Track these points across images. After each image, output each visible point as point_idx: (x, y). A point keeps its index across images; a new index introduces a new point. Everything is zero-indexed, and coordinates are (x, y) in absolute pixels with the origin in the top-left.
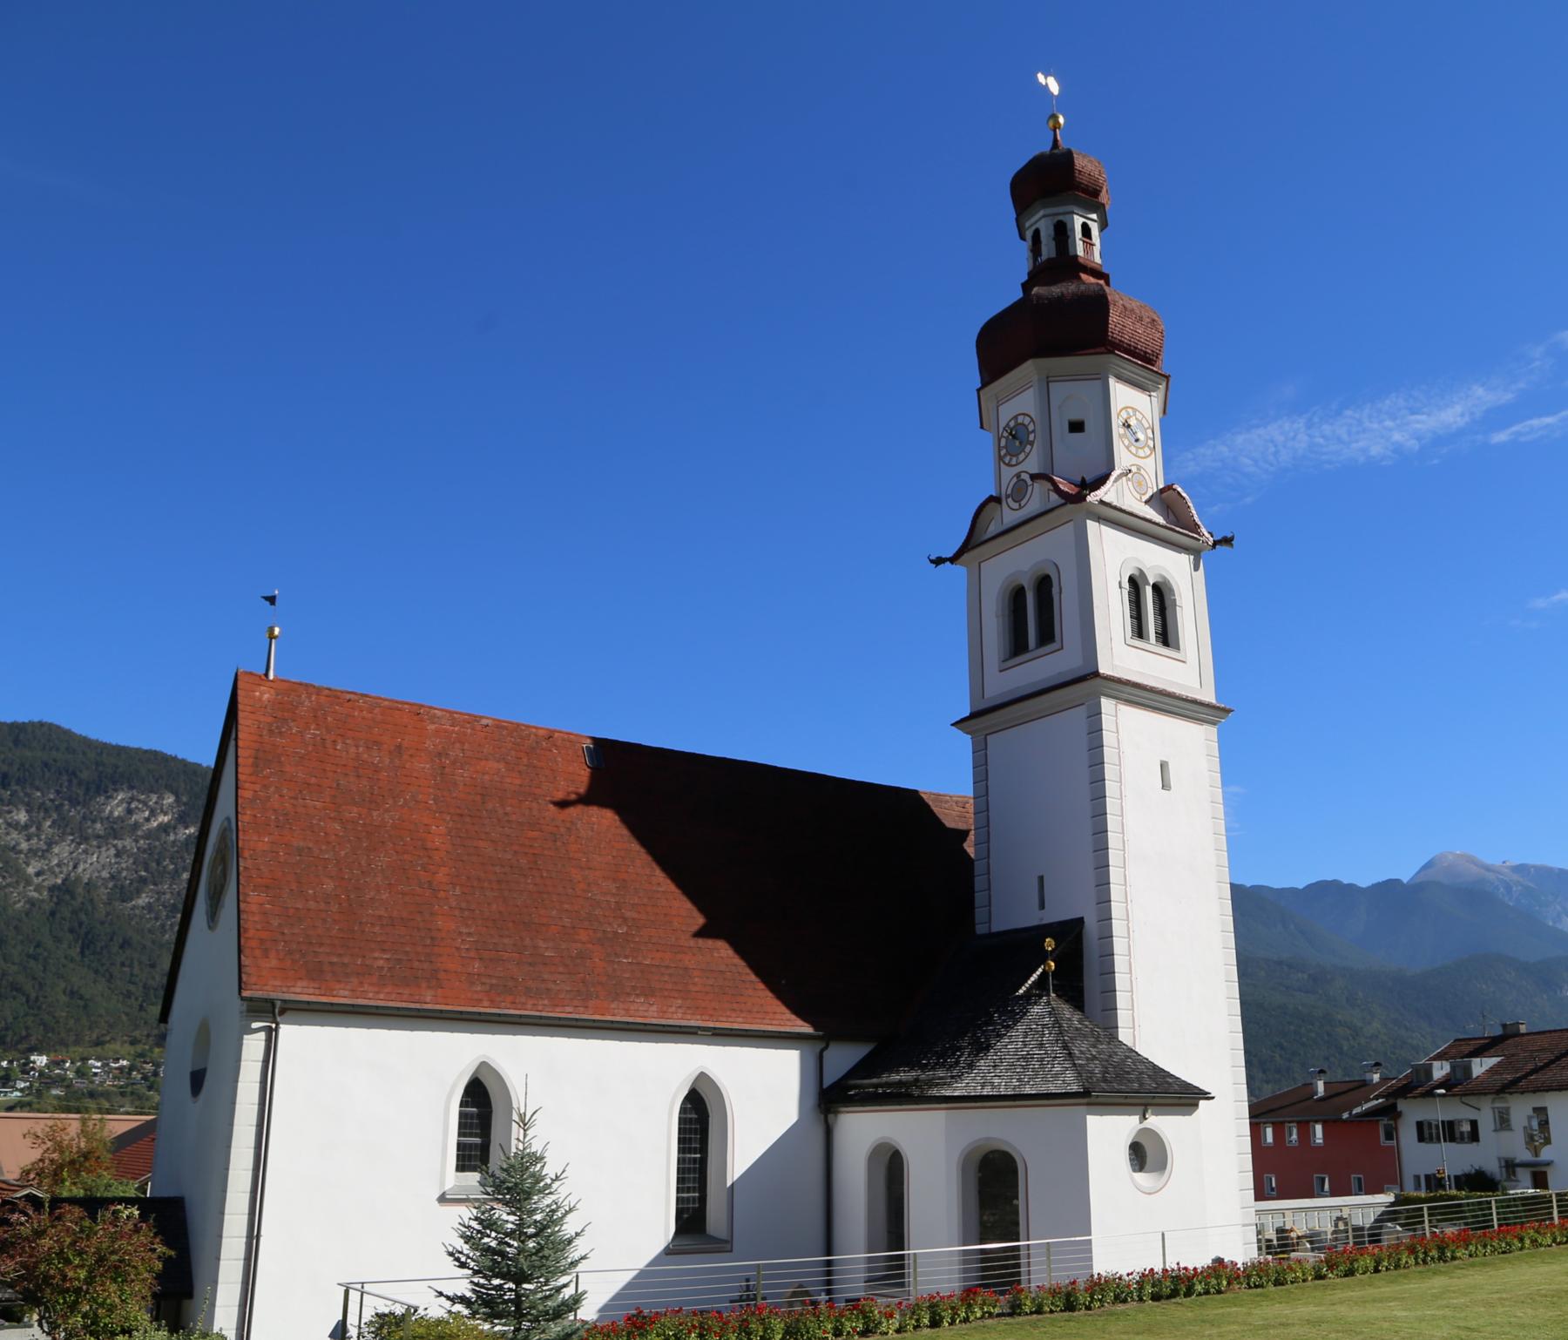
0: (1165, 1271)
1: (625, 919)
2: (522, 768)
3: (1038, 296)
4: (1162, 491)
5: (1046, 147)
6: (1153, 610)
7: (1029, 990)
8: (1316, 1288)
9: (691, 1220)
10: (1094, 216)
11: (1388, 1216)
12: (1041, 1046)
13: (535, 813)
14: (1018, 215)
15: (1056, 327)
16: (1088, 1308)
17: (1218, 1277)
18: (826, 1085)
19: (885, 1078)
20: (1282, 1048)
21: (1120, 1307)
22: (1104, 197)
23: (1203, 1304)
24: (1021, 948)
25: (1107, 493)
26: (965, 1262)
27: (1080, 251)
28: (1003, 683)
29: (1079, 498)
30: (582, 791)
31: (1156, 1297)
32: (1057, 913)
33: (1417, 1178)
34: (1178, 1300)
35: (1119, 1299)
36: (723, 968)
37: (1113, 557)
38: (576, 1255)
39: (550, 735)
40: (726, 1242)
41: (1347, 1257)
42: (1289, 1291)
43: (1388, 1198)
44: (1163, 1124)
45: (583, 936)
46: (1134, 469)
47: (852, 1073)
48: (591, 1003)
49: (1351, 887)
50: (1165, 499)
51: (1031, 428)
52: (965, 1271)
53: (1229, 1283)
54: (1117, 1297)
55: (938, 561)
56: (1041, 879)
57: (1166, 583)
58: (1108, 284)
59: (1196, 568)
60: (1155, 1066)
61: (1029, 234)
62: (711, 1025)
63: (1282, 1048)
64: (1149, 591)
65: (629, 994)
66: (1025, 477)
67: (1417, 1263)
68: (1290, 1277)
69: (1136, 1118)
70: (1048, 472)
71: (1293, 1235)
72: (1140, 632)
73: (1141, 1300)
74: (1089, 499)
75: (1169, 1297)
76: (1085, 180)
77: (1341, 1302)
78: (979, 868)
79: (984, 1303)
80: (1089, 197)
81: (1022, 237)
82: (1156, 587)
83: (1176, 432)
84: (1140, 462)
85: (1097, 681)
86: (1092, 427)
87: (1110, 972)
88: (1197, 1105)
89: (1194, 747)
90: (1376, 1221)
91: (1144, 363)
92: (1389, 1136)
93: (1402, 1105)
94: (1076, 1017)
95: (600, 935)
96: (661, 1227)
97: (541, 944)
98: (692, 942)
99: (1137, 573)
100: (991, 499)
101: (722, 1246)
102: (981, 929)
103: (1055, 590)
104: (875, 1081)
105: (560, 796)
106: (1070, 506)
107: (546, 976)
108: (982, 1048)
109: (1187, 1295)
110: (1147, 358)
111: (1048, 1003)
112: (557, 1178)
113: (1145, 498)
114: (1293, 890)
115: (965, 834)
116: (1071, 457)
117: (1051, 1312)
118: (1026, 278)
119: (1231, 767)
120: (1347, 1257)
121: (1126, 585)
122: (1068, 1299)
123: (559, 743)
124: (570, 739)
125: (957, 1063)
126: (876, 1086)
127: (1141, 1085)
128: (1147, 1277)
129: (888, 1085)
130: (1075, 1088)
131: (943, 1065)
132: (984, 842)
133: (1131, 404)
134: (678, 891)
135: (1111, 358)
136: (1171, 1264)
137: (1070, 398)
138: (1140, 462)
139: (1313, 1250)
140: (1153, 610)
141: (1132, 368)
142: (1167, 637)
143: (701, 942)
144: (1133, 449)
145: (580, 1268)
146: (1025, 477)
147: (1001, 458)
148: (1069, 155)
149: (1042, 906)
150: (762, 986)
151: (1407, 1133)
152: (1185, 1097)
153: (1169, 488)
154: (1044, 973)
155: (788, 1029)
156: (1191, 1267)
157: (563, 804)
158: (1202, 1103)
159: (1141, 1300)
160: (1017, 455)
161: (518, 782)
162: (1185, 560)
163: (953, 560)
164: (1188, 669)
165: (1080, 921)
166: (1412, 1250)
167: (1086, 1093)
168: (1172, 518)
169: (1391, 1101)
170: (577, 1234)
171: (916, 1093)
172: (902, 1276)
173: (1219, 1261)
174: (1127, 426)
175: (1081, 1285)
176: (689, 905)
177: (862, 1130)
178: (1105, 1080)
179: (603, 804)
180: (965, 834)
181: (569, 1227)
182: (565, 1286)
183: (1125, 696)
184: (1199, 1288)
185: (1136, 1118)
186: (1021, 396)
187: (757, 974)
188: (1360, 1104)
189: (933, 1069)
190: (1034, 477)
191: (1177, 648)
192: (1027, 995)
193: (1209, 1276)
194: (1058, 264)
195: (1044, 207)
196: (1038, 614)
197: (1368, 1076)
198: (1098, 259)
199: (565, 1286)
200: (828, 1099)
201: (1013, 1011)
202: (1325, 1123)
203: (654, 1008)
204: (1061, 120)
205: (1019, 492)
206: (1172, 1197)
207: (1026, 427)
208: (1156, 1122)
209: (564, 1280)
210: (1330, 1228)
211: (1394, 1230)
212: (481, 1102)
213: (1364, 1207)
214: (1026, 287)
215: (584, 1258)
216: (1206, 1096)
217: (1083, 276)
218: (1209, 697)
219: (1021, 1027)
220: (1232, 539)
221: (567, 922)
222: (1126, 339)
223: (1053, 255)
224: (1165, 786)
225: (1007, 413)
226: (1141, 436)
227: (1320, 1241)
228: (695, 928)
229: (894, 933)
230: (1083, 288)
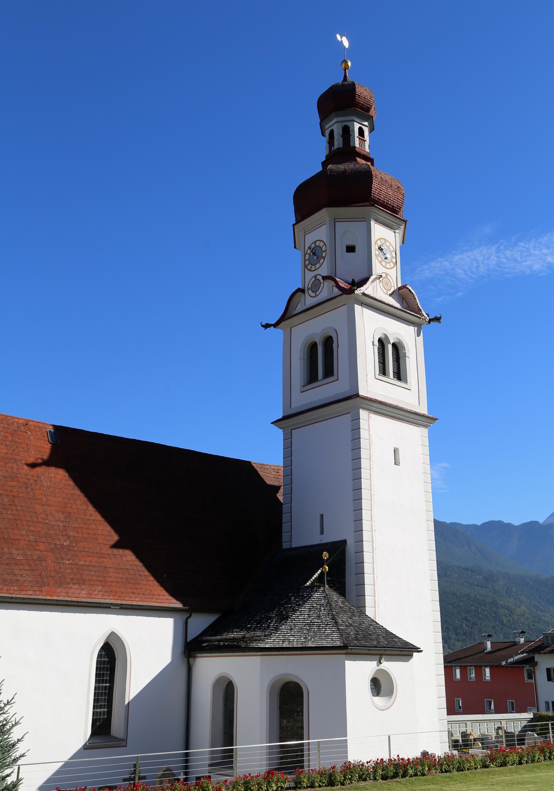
0: (390, 760)
1: (69, 537)
2: (8, 443)
3: (331, 170)
4: (400, 289)
5: (340, 80)
6: (391, 359)
7: (312, 583)
8: (483, 773)
9: (101, 727)
10: (366, 123)
11: (529, 727)
12: (319, 617)
13: (15, 470)
14: (322, 120)
15: (341, 188)
16: (343, 784)
17: (423, 765)
18: (188, 640)
19: (224, 636)
20: (467, 620)
21: (362, 784)
22: (372, 112)
23: (413, 783)
24: (309, 556)
25: (368, 289)
26: (270, 754)
27: (357, 144)
28: (304, 398)
29: (351, 291)
30: (45, 457)
31: (384, 778)
32: (330, 537)
33: (547, 703)
34: (398, 779)
35: (362, 778)
36: (128, 567)
37: (370, 327)
38: (18, 754)
39: (27, 423)
40: (123, 740)
41: (504, 753)
42: (466, 775)
43: (529, 715)
44: (392, 667)
45: (42, 547)
46: (384, 275)
47: (206, 632)
48: (44, 589)
49: (509, 526)
50: (401, 294)
51: (324, 249)
52: (270, 759)
53: (429, 769)
54: (360, 777)
55: (267, 326)
56: (322, 516)
57: (400, 343)
58: (373, 165)
59: (418, 335)
60: (387, 631)
61: (327, 133)
62: (119, 602)
63: (467, 620)
64: (390, 347)
65: (68, 583)
66: (320, 278)
67: (545, 759)
68: (467, 765)
69: (375, 663)
70: (333, 275)
71: (471, 737)
72: (383, 371)
73: (375, 779)
74: (356, 292)
75: (393, 777)
76: (361, 101)
77: (498, 784)
78: (285, 509)
79: (278, 781)
80: (364, 111)
81: (323, 135)
82: (394, 346)
83: (408, 256)
84: (388, 271)
85: (358, 399)
86: (358, 249)
87: (361, 573)
88: (412, 656)
89: (414, 440)
90: (521, 731)
91: (392, 212)
92: (530, 677)
93: (537, 658)
94: (341, 600)
95: (52, 546)
96: (83, 731)
97: (15, 551)
98: (110, 551)
99: (383, 337)
100: (299, 290)
101: (120, 743)
102: (285, 546)
103: (335, 345)
104: (219, 637)
105: (31, 460)
106: (345, 296)
107: (16, 572)
108: (283, 618)
109: (404, 776)
110: (394, 210)
111: (324, 591)
112: (8, 703)
113: (390, 292)
114: (474, 526)
115: (277, 488)
116: (347, 268)
117: (320, 786)
118: (324, 159)
119: (436, 454)
120: (504, 753)
121: (376, 343)
122: (330, 778)
123: (32, 428)
124: (39, 426)
125: (268, 627)
126: (219, 641)
127: (378, 642)
128: (379, 763)
129: (226, 640)
130: (338, 644)
131: (260, 628)
132: (289, 493)
133: (383, 236)
134: (102, 520)
135: (373, 209)
136: (394, 756)
137: (348, 232)
138: (388, 271)
139: (483, 748)
140: (391, 359)
141: (384, 215)
142: (399, 375)
143: (115, 551)
144: (384, 264)
145: (19, 762)
146: (320, 278)
147: (306, 266)
148: (353, 85)
149: (322, 532)
150: (152, 578)
151: (541, 675)
152: (405, 650)
153: (404, 287)
154: (322, 573)
155: (167, 605)
156: (406, 758)
157: (33, 466)
158: (415, 654)
159: (375, 779)
160: (315, 265)
161: (5, 451)
162: (411, 330)
163: (275, 325)
164: (412, 394)
165: (345, 542)
166: (542, 751)
167: (345, 647)
168: (406, 305)
169: (531, 655)
170: (19, 740)
171: (243, 645)
172: (232, 762)
173: (425, 754)
174: (380, 249)
175: (339, 769)
176: (109, 528)
177: (211, 668)
178: (357, 639)
179: (58, 466)
180: (277, 488)
181: (14, 735)
182: (8, 776)
183: (374, 409)
184: (411, 772)
185: (375, 663)
186: (320, 228)
187: (149, 571)
188: (513, 657)
189: (254, 630)
190: (324, 278)
191: (406, 382)
192: (312, 586)
193: (417, 764)
194: (343, 152)
195: (337, 116)
196: (324, 359)
197: (517, 639)
198: (367, 150)
199: (8, 776)
200: (190, 648)
201: (303, 595)
202: (491, 667)
203: (84, 592)
204: (349, 64)
205: (315, 287)
206: (399, 713)
207: (321, 248)
208: (386, 665)
209: (7, 771)
210: (494, 734)
211: (533, 737)
212: (538, 711)
213: (515, 721)
214: (325, 164)
215: (22, 756)
216: (417, 650)
217: (358, 159)
218: (423, 410)
219: (307, 606)
220: (440, 318)
221: (32, 538)
222: (382, 198)
223: (341, 146)
224: (397, 463)
225: (310, 239)
226: (388, 256)
227: (488, 743)
228: (112, 542)
229: (233, 548)
230: (357, 166)
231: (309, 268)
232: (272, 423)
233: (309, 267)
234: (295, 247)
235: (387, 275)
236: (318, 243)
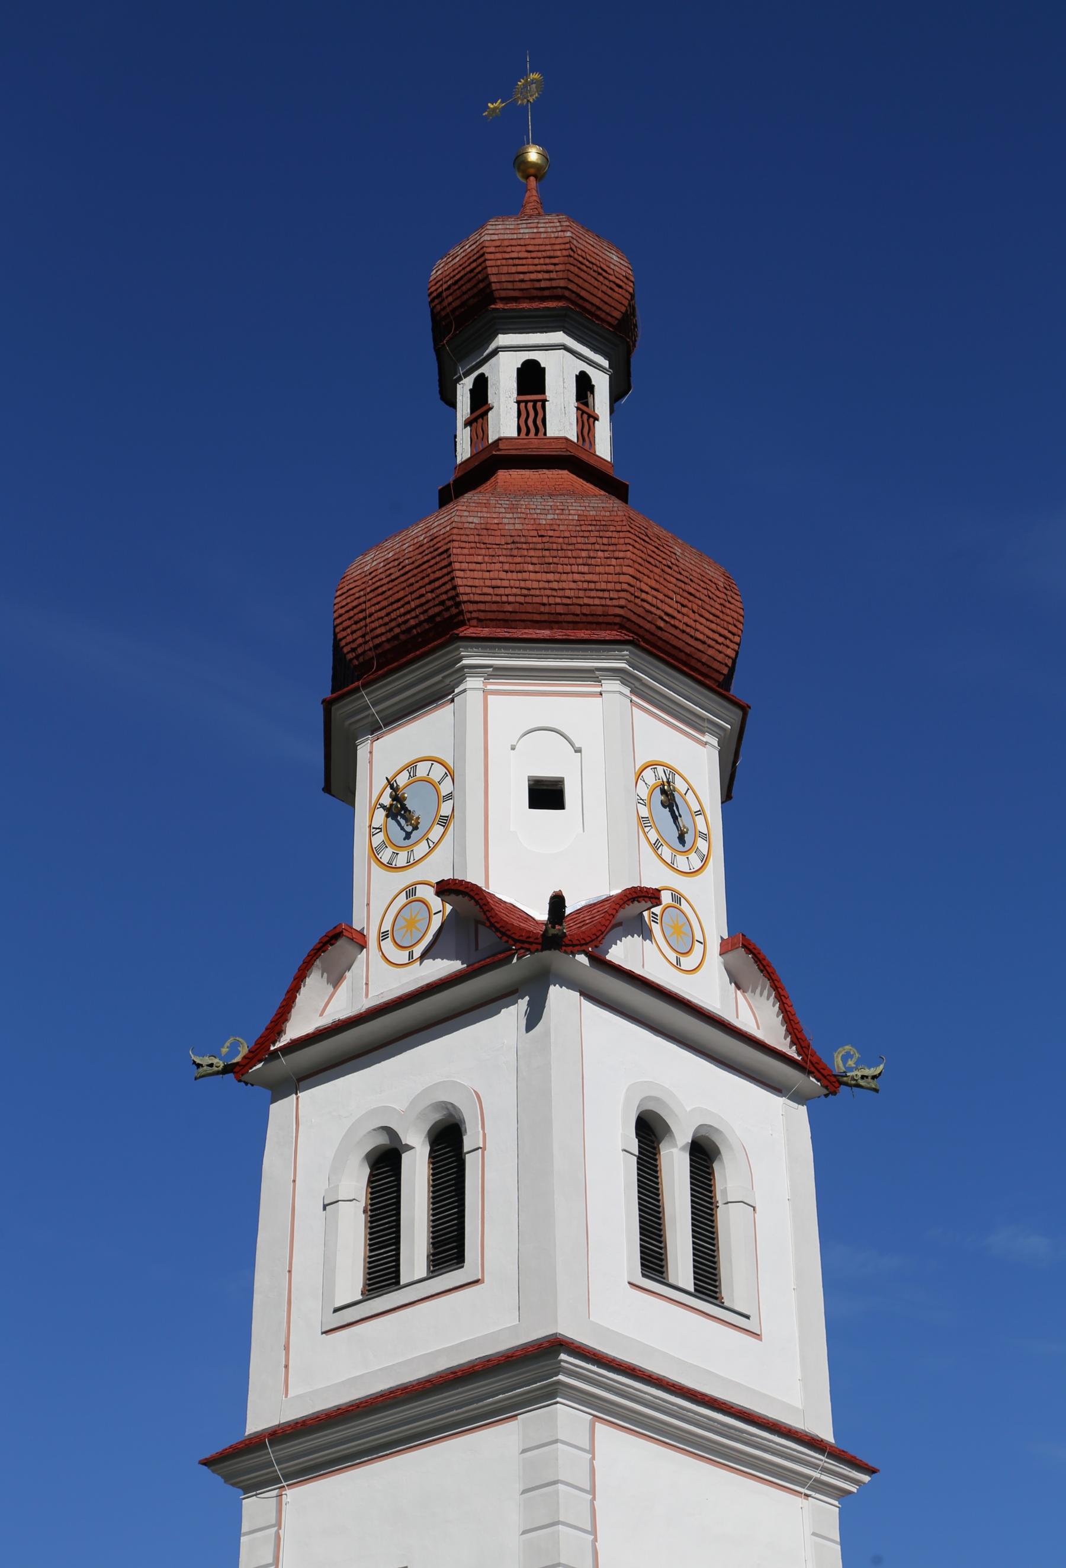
46: (666, 898)
51: (446, 788)
164: (775, 1348)
207: (435, 786)
231: (660, 769)
232: (206, 1463)
233: (386, 856)
234: (327, 789)
235: (677, 897)
236: (422, 770)
